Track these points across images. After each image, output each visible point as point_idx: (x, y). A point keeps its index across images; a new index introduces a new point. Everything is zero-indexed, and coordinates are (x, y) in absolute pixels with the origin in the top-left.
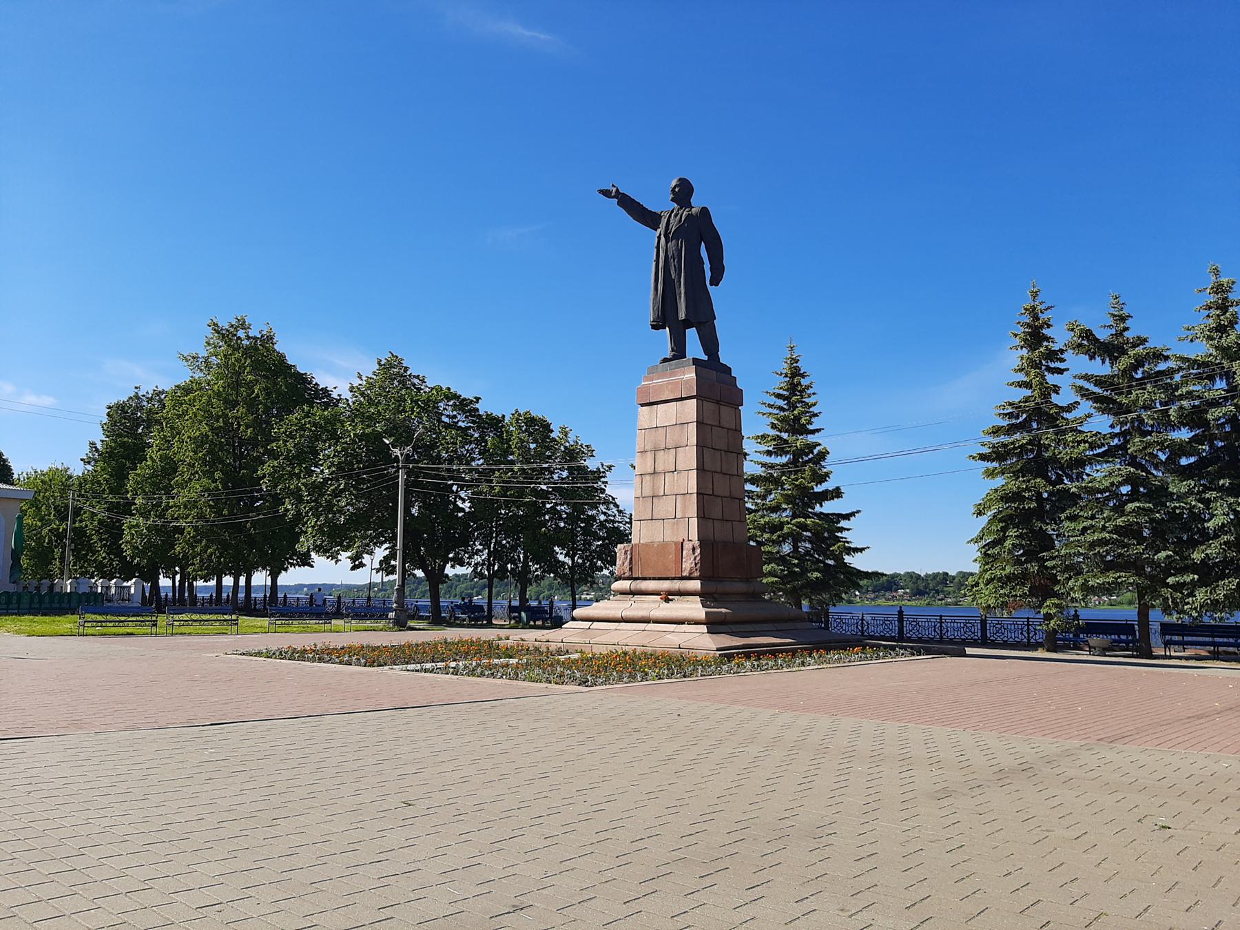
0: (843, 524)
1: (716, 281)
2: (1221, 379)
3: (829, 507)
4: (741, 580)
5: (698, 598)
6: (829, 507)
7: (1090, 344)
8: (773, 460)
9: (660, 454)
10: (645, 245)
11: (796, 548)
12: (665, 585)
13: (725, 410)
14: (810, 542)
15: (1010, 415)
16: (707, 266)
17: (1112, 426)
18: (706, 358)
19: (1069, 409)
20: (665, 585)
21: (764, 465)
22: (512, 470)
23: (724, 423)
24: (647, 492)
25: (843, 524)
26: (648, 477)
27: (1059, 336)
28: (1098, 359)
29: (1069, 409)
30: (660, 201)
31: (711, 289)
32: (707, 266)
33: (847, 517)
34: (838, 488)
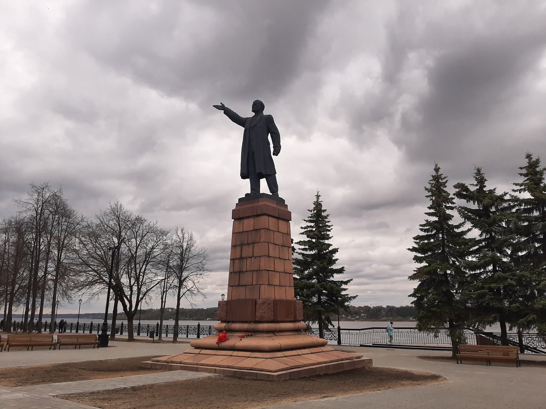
0: (344, 286)
1: (276, 153)
2: (536, 210)
3: (337, 277)
4: (291, 322)
5: (241, 130)
6: (337, 277)
7: (463, 192)
8: (308, 252)
9: (245, 248)
10: (237, 133)
11: (319, 299)
12: (245, 326)
13: (281, 223)
14: (327, 296)
15: (425, 231)
16: (272, 146)
17: (481, 235)
18: (271, 194)
19: (458, 227)
20: (245, 326)
21: (303, 255)
22: (495, 261)
23: (280, 230)
24: (237, 269)
25: (344, 286)
26: (237, 261)
27: (451, 190)
28: (472, 202)
29: (458, 227)
30: (246, 112)
31: (274, 157)
32: (272, 146)
33: (346, 283)
34: (343, 268)
